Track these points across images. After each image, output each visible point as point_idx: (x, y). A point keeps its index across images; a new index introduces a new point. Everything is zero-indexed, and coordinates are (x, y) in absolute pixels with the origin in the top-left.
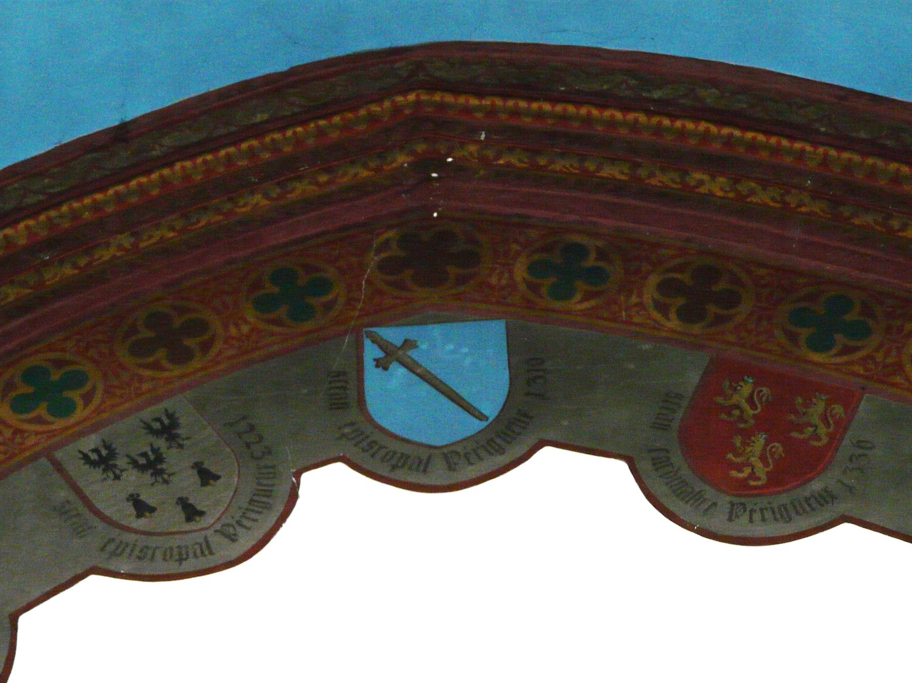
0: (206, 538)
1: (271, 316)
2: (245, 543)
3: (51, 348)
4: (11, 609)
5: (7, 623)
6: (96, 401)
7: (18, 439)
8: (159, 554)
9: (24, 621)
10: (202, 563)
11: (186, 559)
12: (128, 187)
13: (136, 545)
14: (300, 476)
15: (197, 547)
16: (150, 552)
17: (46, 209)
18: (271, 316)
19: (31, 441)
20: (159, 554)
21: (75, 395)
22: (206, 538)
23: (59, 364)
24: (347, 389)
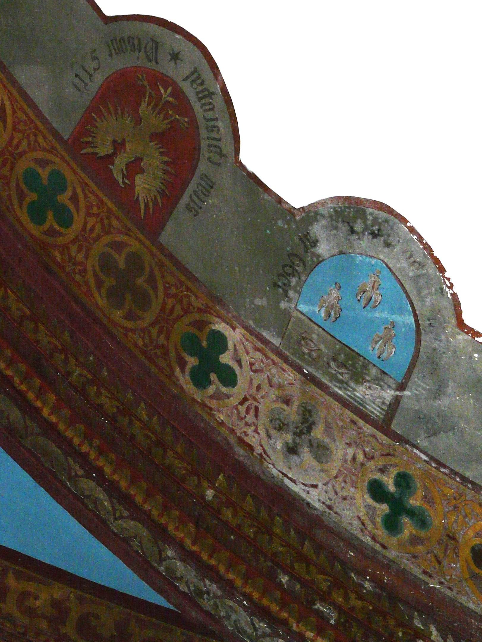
0: (184, 80)
1: (71, 207)
2: (187, 47)
3: (88, 293)
4: (100, 22)
5: (114, 25)
6: (119, 238)
7: (22, 127)
8: (210, 115)
9: (109, 12)
10: (207, 74)
11: (208, 91)
12: (14, 375)
13: (207, 138)
14: (108, 17)
15: (195, 86)
16: (211, 123)
17: (59, 433)
18: (71, 207)
19: (171, 279)
20: (210, 115)
21: (44, 174)
22: (184, 80)
23: (22, 196)
24: (194, 191)
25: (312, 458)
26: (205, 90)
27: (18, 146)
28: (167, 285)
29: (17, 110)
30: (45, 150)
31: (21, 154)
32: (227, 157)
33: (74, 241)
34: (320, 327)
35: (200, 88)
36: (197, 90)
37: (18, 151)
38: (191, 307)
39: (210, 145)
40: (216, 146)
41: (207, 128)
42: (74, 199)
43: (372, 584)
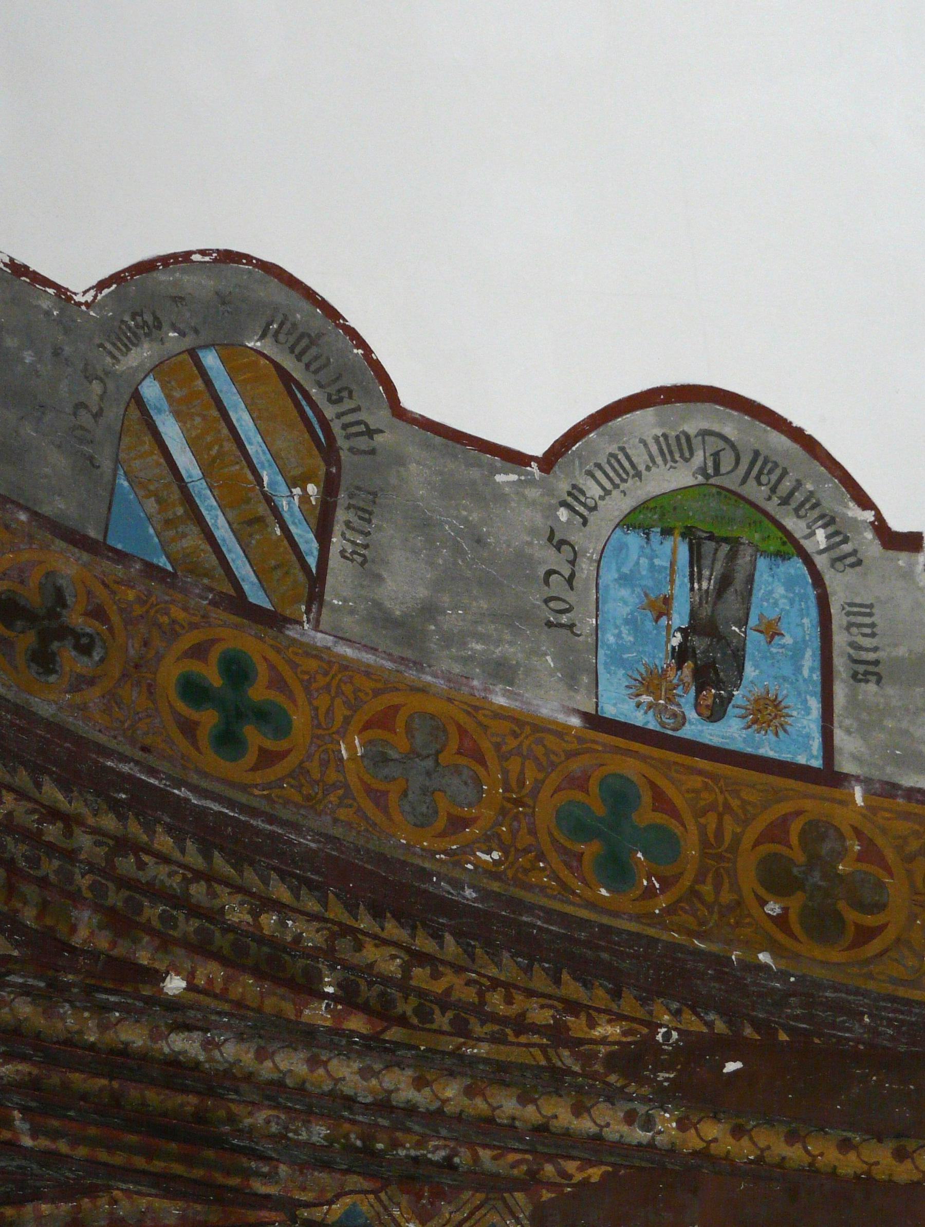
18: (279, 699)
25: (176, 677)
26: (302, 336)
27: (521, 783)
28: (306, 677)
29: (297, 660)
30: (194, 626)
31: (535, 792)
32: (567, 561)
33: (700, 877)
34: (597, 592)
35: (292, 340)
36: (289, 344)
37: (525, 791)
38: (360, 694)
39: (345, 427)
40: (358, 423)
41: (330, 400)
42: (278, 682)
43: (183, 1036)
